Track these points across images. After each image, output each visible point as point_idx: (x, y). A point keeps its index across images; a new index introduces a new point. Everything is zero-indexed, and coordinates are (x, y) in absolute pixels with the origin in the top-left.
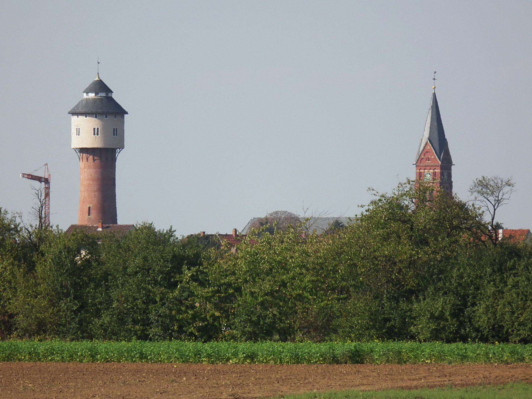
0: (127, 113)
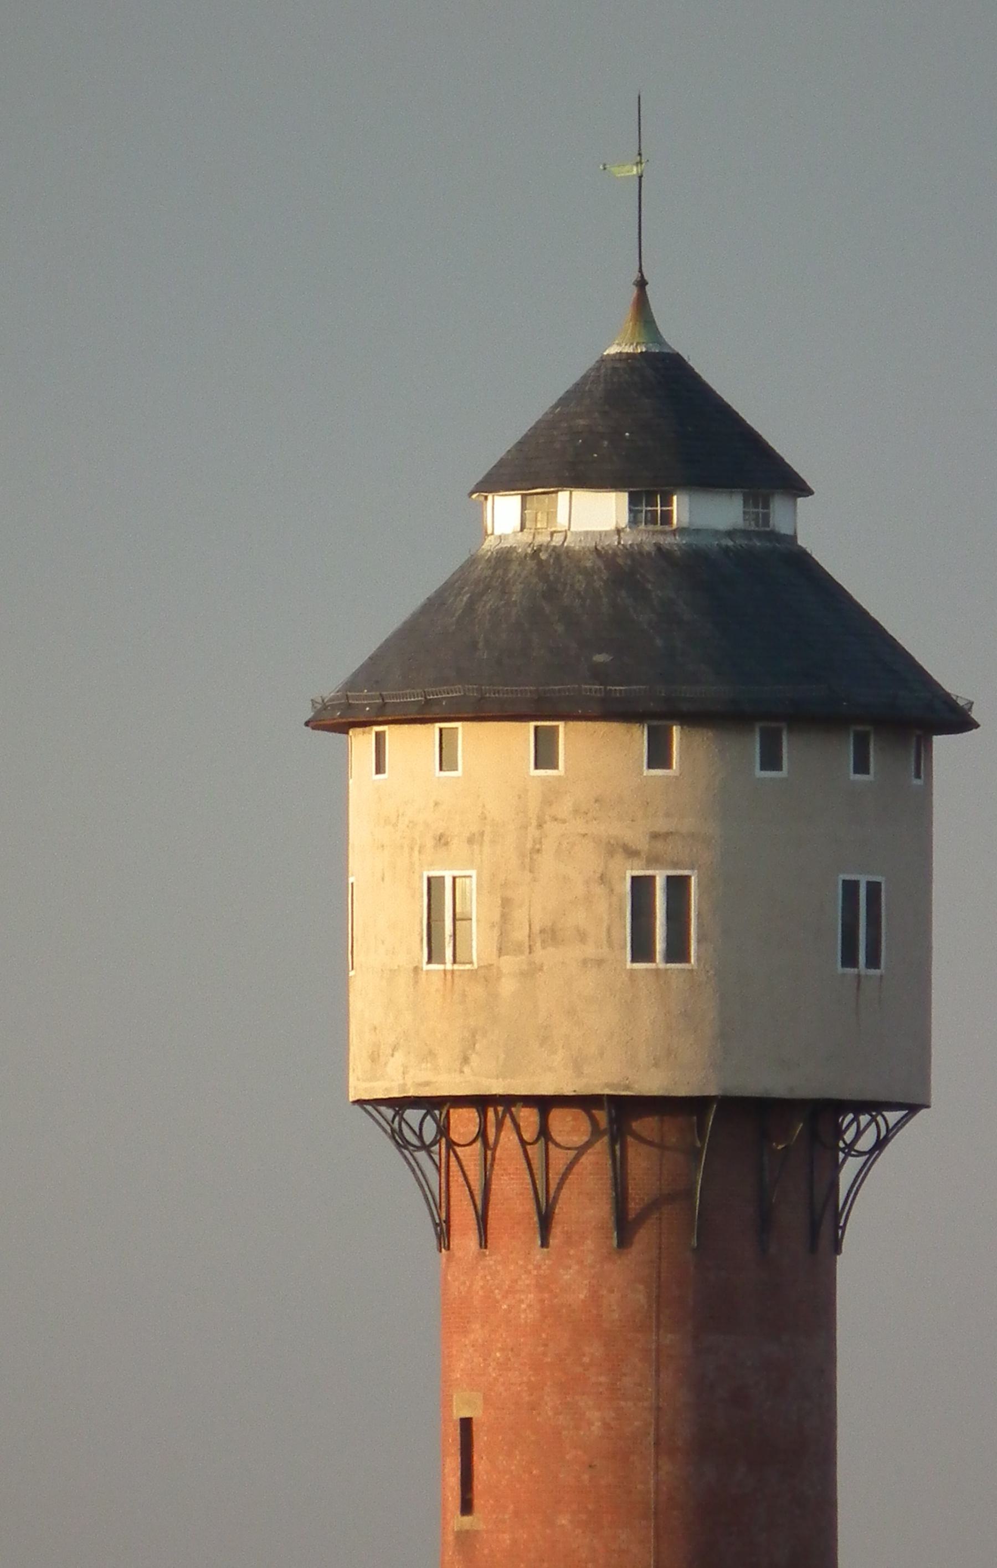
0: (957, 719)
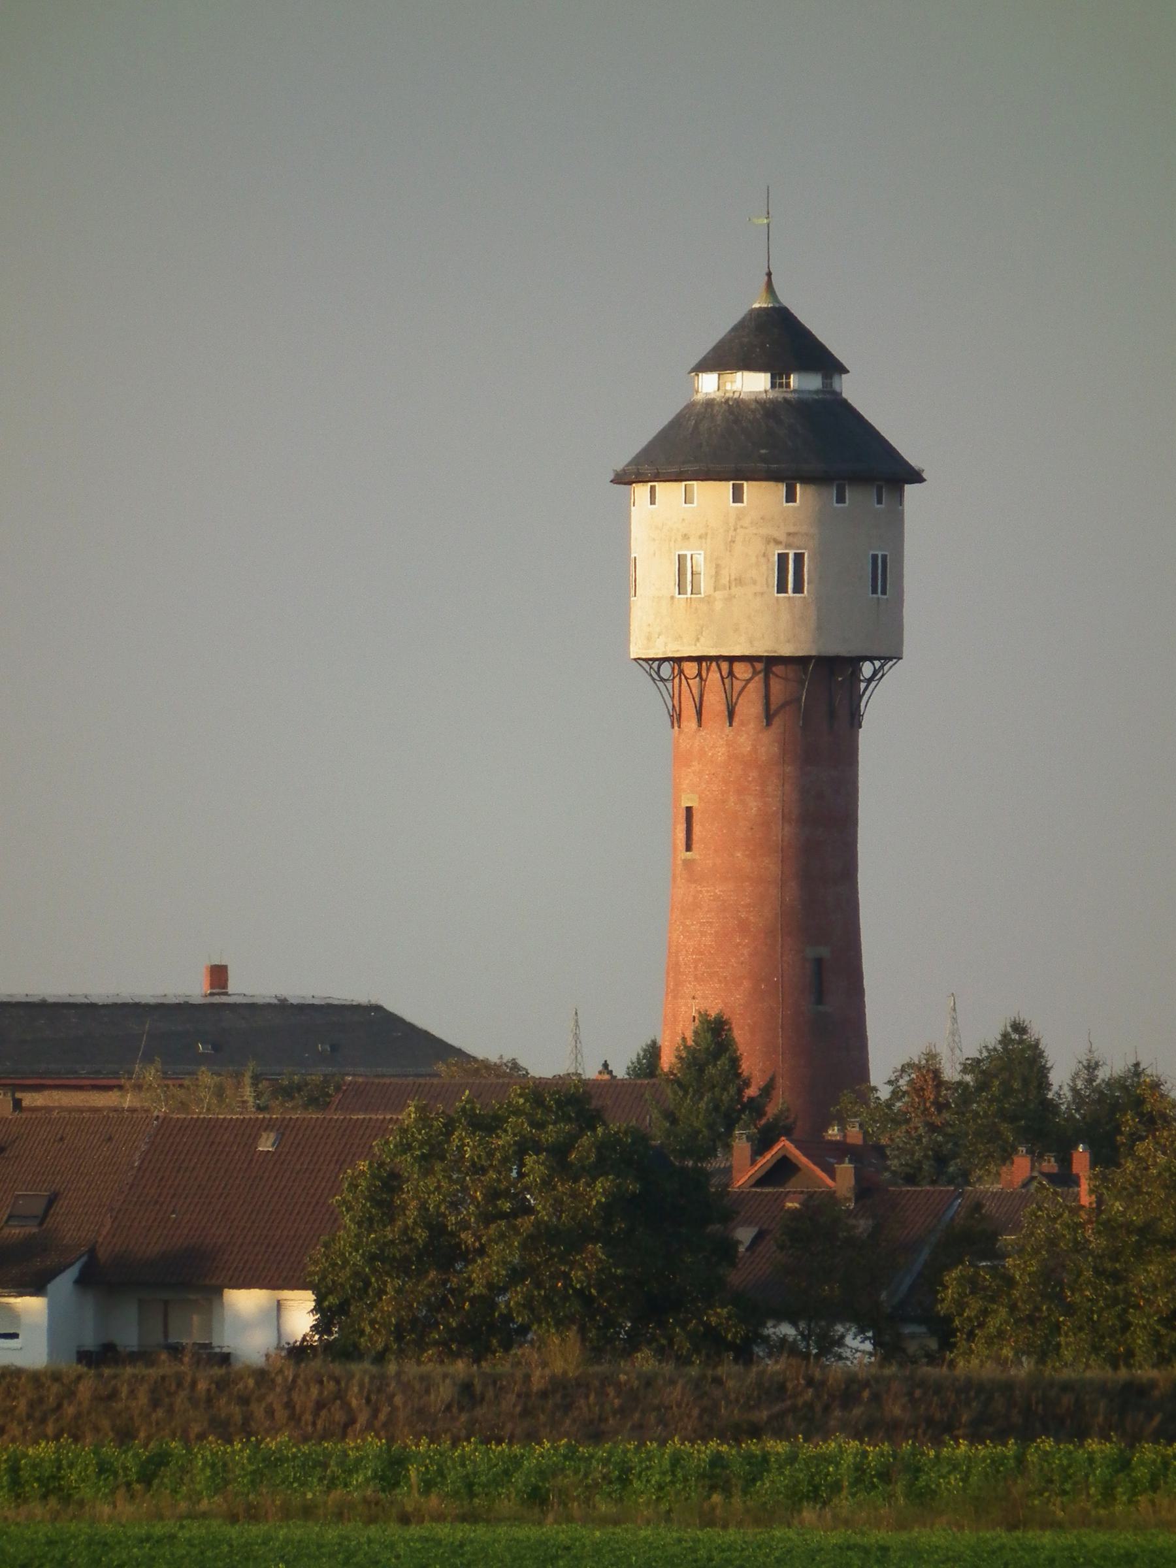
0: (916, 477)
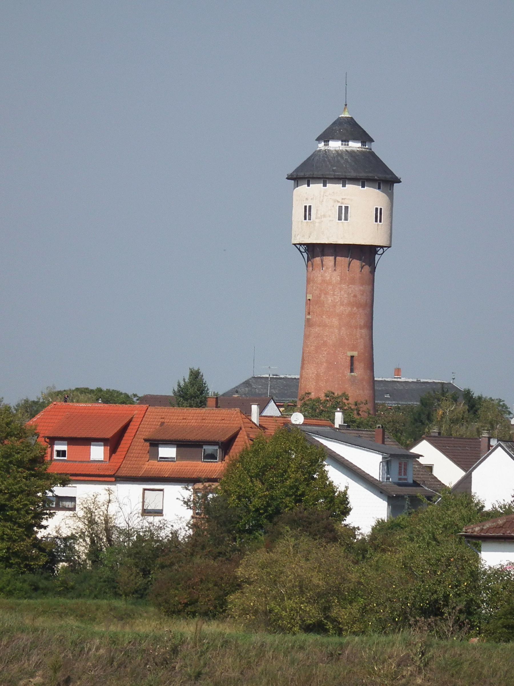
0: (399, 181)
